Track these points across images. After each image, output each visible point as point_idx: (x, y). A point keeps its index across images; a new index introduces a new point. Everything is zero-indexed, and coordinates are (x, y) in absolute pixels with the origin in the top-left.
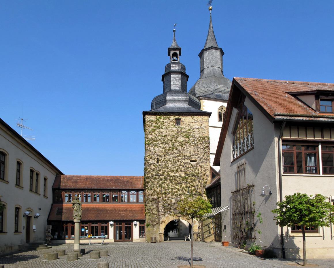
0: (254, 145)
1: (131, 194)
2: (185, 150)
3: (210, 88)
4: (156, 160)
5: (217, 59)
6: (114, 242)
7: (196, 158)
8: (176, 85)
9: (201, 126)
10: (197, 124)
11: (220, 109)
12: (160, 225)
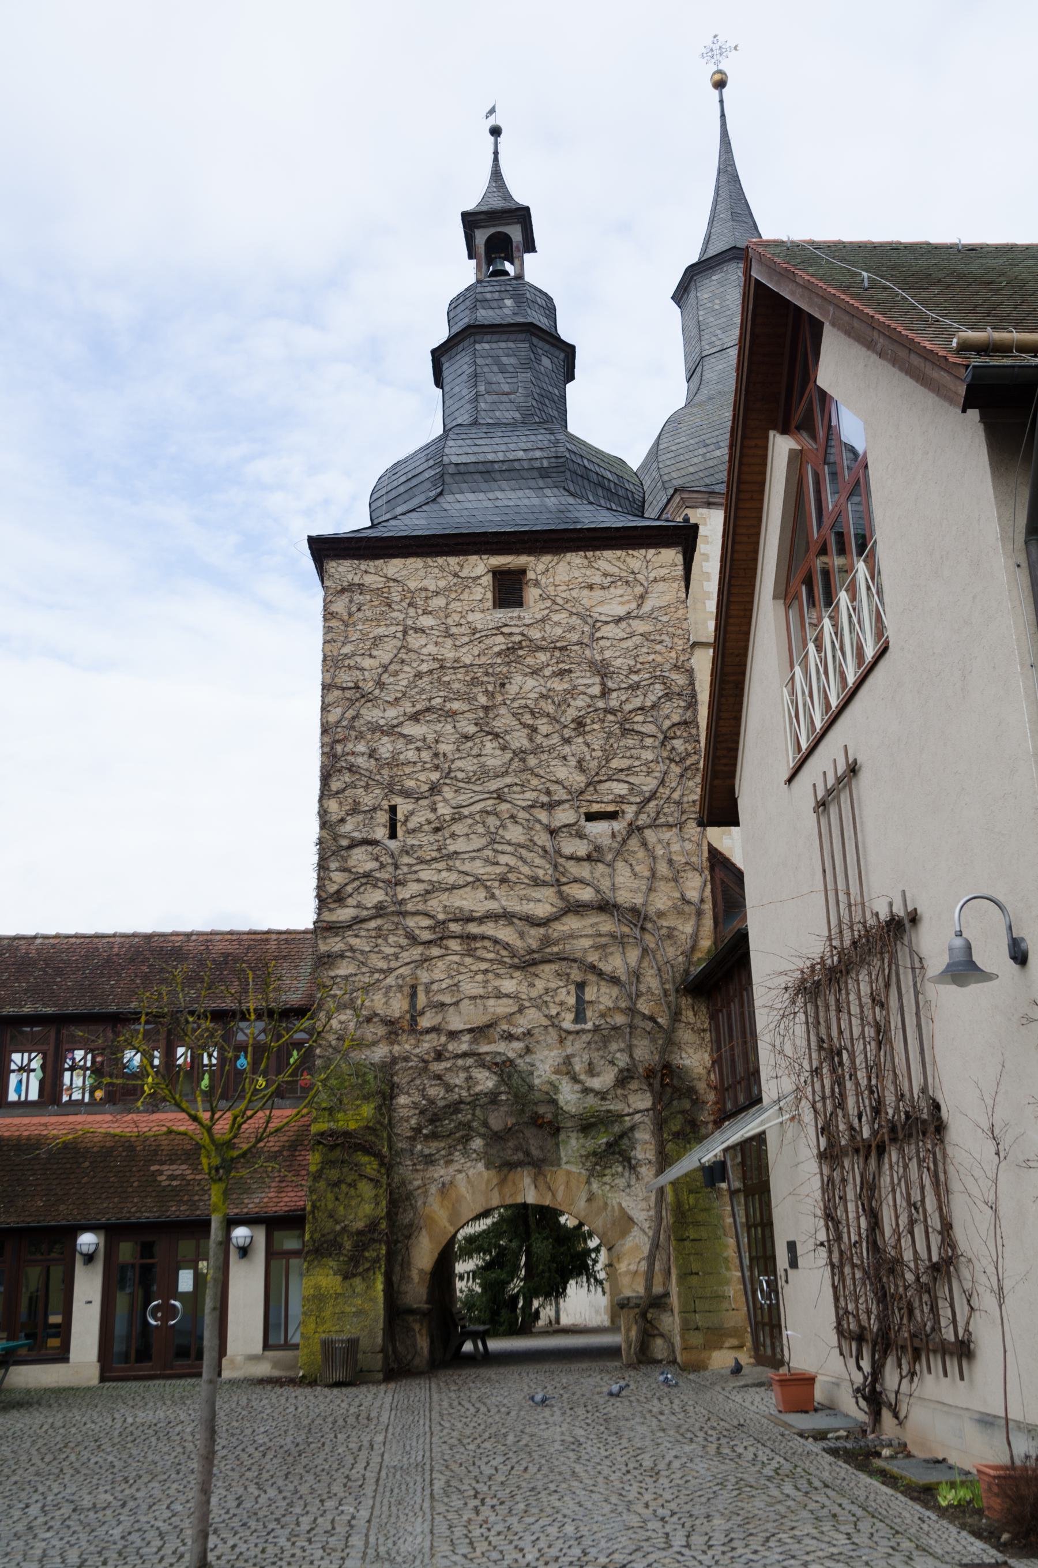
2: (552, 749)
4: (383, 817)
6: (103, 1379)
7: (621, 800)
8: (504, 398)
9: (639, 606)
10: (620, 592)
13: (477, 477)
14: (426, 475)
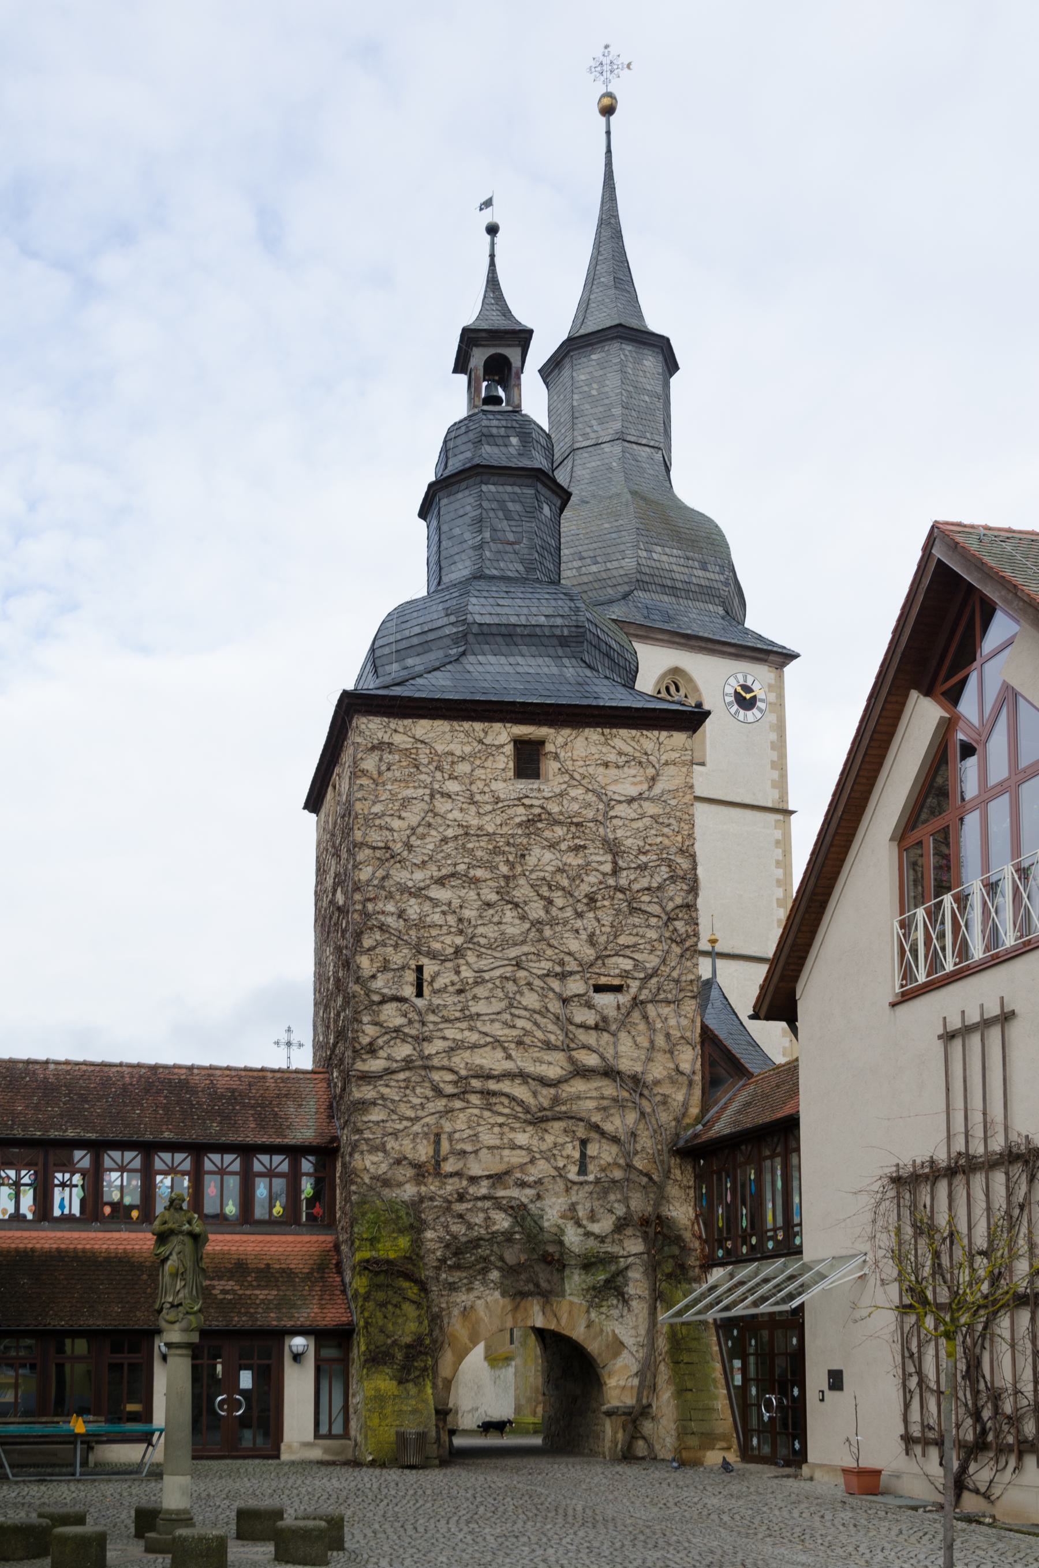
1: (261, 1175)
2: (566, 922)
3: (609, 565)
4: (410, 976)
5: (647, 398)
7: (625, 974)
9: (650, 788)
10: (633, 772)
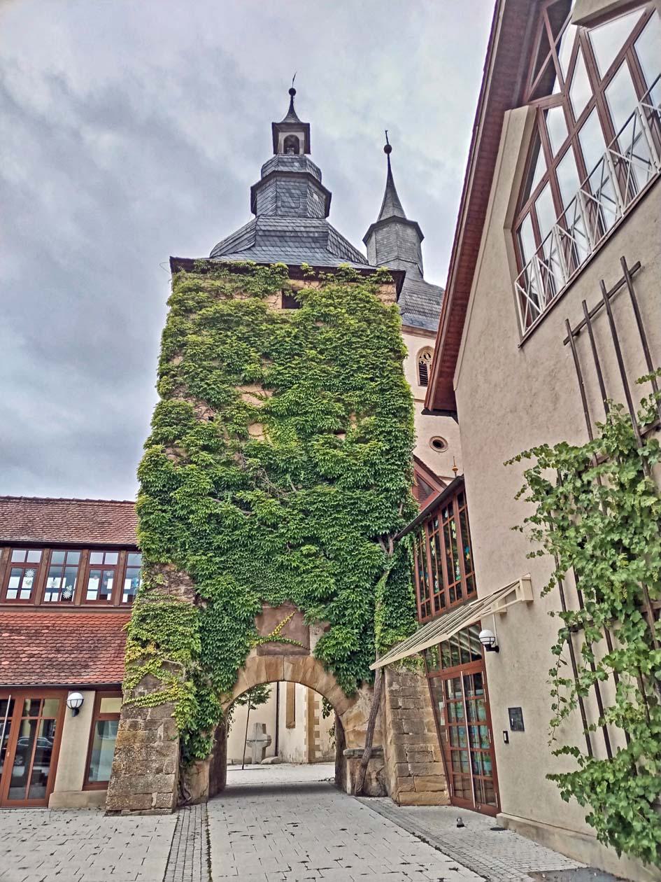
0: (567, 352)
8: (292, 210)
11: (422, 356)
12: (285, 758)
13: (276, 239)
14: (246, 237)
